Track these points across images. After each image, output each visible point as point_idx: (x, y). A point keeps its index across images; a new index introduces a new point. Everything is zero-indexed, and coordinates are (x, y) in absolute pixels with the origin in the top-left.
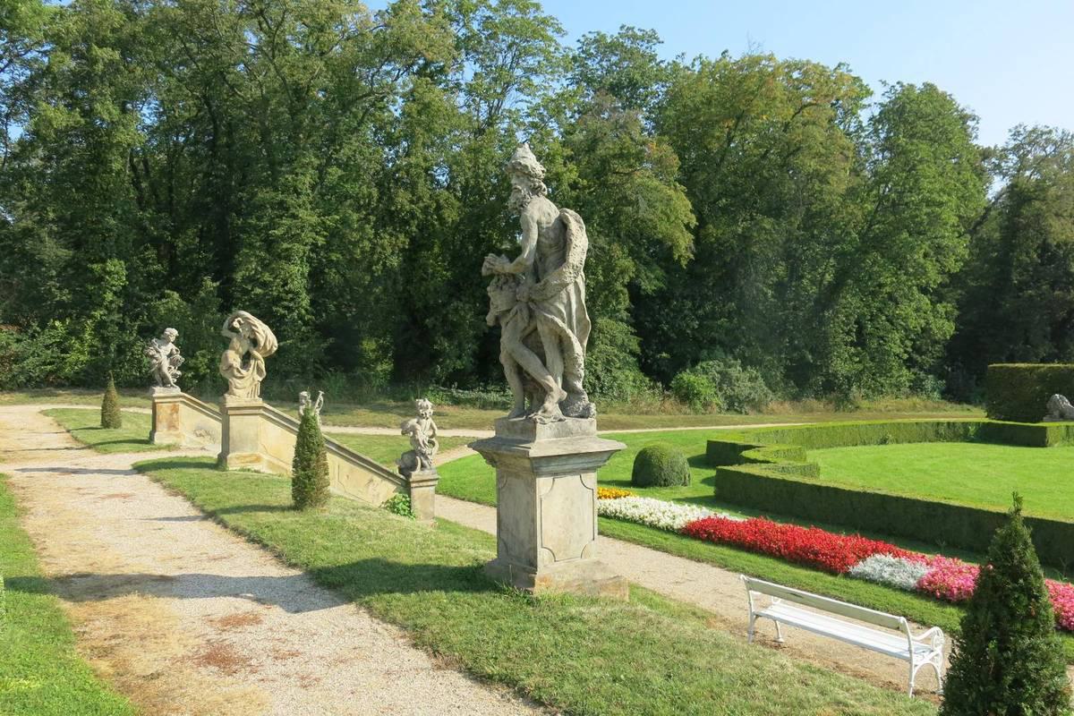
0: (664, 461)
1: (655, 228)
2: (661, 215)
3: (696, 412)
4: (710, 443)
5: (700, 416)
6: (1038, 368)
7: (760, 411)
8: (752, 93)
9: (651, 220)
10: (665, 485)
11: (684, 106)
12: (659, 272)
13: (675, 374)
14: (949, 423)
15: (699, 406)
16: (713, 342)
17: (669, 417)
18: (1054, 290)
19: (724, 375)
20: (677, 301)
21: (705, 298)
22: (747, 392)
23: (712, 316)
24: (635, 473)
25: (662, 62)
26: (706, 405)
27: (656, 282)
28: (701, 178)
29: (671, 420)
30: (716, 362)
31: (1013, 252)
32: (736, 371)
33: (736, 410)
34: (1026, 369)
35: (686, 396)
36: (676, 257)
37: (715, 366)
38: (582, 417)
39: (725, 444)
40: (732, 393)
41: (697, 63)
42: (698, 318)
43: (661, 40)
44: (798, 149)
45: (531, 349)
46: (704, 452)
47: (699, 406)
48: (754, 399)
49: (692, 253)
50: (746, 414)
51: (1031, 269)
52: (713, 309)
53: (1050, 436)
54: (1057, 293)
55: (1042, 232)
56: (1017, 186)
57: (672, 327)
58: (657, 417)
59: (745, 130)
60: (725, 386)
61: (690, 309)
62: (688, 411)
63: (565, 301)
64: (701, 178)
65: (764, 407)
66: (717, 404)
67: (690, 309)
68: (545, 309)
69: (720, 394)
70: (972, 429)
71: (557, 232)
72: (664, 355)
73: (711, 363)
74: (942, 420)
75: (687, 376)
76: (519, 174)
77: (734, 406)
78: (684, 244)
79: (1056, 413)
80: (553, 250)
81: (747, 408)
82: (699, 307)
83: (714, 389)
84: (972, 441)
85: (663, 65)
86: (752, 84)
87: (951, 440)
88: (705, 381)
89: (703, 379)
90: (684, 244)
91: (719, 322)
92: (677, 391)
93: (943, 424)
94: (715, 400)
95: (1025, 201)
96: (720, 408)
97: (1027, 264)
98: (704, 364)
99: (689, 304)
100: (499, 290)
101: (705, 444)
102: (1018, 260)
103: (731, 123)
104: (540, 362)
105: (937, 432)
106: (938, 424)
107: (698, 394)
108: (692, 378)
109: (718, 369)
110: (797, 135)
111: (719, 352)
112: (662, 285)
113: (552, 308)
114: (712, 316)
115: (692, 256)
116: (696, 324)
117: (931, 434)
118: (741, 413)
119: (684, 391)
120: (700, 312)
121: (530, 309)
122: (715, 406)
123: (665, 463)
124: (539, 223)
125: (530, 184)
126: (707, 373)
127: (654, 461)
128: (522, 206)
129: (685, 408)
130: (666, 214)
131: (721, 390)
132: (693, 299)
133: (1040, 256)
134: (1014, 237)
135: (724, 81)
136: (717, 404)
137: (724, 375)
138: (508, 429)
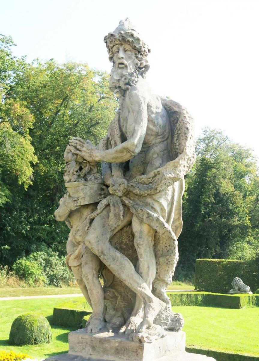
0: (34, 325)
1: (15, 161)
2: (19, 153)
3: (29, 285)
4: (55, 310)
5: (32, 288)
6: (223, 261)
7: (69, 285)
8: (73, 85)
9: (12, 156)
10: (35, 343)
11: (28, 88)
12: (7, 192)
13: (15, 261)
14: (187, 294)
15: (31, 282)
16: (39, 239)
17: (12, 289)
18: (221, 218)
19: (48, 262)
20: (17, 211)
21: (35, 211)
22: (61, 273)
23: (39, 222)
24: (12, 335)
25: (14, 57)
26: (36, 281)
27: (5, 198)
28: (38, 133)
29: (14, 292)
30: (43, 253)
31: (202, 196)
32: (54, 259)
33: (54, 285)
34: (216, 262)
35: (23, 275)
36: (20, 183)
37: (42, 255)
38: (171, 329)
39: (66, 311)
40: (52, 274)
41: (35, 63)
42: (31, 223)
43: (15, 43)
44: (98, 123)
45: (121, 249)
46: (52, 314)
47: (31, 282)
48: (65, 278)
49: (32, 181)
50: (61, 287)
51: (210, 206)
52: (39, 218)
53: (242, 302)
54: (223, 220)
55: (217, 187)
56: (205, 160)
57: (12, 230)
58: (4, 289)
59: (66, 107)
60: (48, 269)
61: (25, 218)
62: (25, 285)
63: (169, 198)
64: (38, 133)
65: (71, 283)
66: (43, 281)
67: (25, 218)
68: (147, 205)
69: (44, 274)
70: (200, 298)
71: (165, 119)
72: (7, 247)
73: (39, 253)
74: (183, 293)
75: (24, 262)
76: (128, 47)
77: (53, 282)
78: (26, 176)
79: (237, 288)
80: (158, 140)
81: (61, 283)
82: (30, 217)
83: (41, 271)
84: (200, 305)
85: (15, 60)
86: (73, 79)
87: (188, 305)
88: (36, 266)
89: (35, 264)
90: (26, 176)
91: (43, 227)
92: (17, 271)
93: (184, 295)
94: (42, 278)
95: (209, 168)
96: (44, 283)
97: (209, 203)
98: (35, 254)
99: (25, 215)
100: (82, 181)
101: (53, 310)
102: (205, 200)
103: (60, 102)
104: (133, 267)
105: (181, 300)
106: (182, 295)
107: (31, 274)
108: (28, 263)
109: (44, 257)
110: (97, 115)
111: (44, 246)
112: (8, 200)
113: (156, 206)
114: (39, 222)
115: (31, 183)
116: (28, 227)
117: (178, 301)
118: (57, 286)
119: (22, 271)
120: (31, 220)
121: (124, 205)
122: (41, 282)
123: (36, 328)
124: (149, 106)
125: (137, 61)
126: (36, 260)
127: (28, 326)
128: (128, 84)
129: (22, 283)
130: (21, 153)
131: (45, 271)
132: (27, 211)
133: (215, 199)
134: (203, 187)
135: (54, 76)
136: (43, 281)
137: (48, 262)
138: (93, 348)
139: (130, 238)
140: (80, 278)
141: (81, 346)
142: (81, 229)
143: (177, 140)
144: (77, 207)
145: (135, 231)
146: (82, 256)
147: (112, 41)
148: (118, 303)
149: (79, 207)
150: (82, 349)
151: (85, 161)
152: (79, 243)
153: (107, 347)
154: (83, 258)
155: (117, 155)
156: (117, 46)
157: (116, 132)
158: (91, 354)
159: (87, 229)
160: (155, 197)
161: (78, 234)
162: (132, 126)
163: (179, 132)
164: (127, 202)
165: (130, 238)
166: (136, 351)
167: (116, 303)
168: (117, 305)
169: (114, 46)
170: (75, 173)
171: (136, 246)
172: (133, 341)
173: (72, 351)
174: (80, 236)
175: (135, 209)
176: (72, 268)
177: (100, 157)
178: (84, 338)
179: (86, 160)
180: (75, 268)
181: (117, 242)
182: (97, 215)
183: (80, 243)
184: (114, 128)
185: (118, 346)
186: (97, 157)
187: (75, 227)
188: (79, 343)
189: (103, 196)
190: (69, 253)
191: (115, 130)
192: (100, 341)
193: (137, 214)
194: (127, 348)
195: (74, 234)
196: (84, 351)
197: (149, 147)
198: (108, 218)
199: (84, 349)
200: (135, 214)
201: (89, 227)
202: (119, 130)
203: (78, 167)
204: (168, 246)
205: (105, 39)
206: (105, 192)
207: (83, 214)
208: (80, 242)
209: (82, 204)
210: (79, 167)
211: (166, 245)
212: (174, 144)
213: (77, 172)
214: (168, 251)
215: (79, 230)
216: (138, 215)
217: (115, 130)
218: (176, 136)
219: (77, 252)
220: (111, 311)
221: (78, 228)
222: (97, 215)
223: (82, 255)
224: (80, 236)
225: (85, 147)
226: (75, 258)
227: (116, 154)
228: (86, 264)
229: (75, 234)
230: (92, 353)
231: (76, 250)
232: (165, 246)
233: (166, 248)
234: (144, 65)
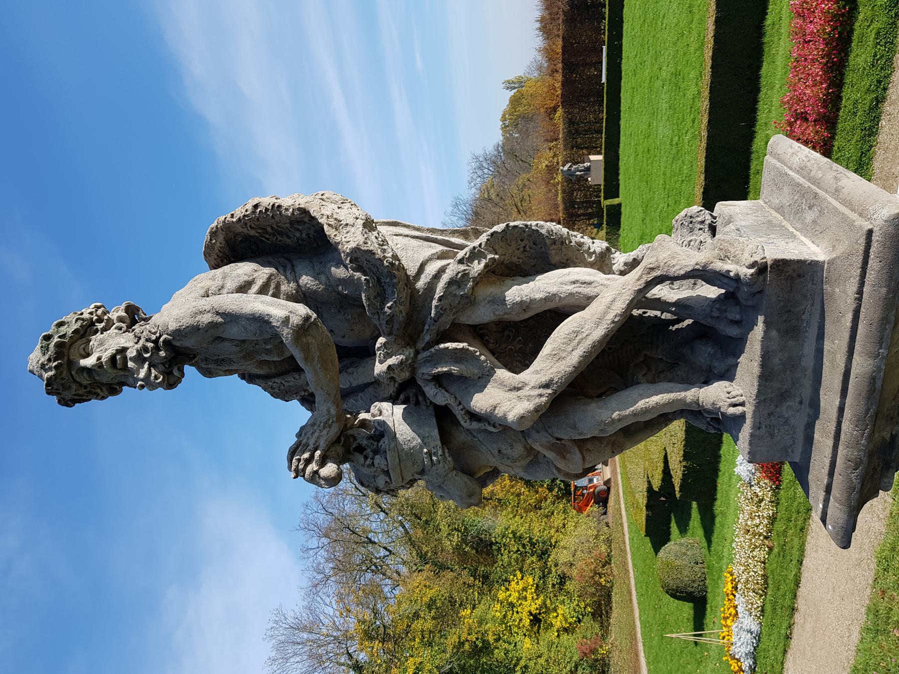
138: (783, 396)
139: (511, 334)
140: (610, 446)
141: (779, 430)
142: (494, 446)
143: (289, 237)
144: (447, 455)
145: (492, 315)
146: (558, 439)
147: (62, 384)
148: (660, 357)
149: (446, 451)
150: (786, 427)
151: (342, 439)
152: (530, 450)
153: (780, 360)
154: (562, 437)
155: (316, 359)
156: (73, 373)
157: (291, 384)
158: (801, 403)
159: (494, 427)
160: (412, 271)
161: (509, 451)
162: (248, 327)
163: (269, 229)
164: (427, 338)
165: (511, 334)
166: (791, 278)
167: (661, 359)
168: (664, 358)
169: (75, 381)
170: (369, 461)
171: (527, 316)
172: (760, 292)
173: (793, 452)
174: (512, 446)
175: (442, 314)
176: (588, 466)
177: (330, 404)
178: (760, 423)
179: (339, 438)
180: (587, 458)
181: (520, 362)
182: (460, 404)
183: (528, 447)
184: (282, 388)
185: (778, 330)
186: (328, 411)
187: (494, 460)
188: (772, 436)
189: (420, 399)
190: (554, 474)
191: (286, 384)
192: (766, 380)
193: (451, 309)
194: (782, 304)
195: (509, 462)
196: (792, 421)
197: (304, 295)
198: (466, 378)
199: (786, 422)
200: (454, 314)
201: (489, 424)
202: (284, 377)
203: (357, 455)
204: (523, 244)
205: (68, 406)
206: (411, 395)
207: (464, 444)
208: (525, 447)
209: (439, 443)
210: (356, 454)
211: (522, 249)
212: (300, 245)
213: (366, 458)
214: (534, 244)
215: (499, 451)
216: (455, 307)
217: (286, 384)
218: (279, 238)
219: (550, 455)
220: (678, 373)
221: (496, 453)
222: (460, 404)
223: (555, 441)
224: (512, 446)
225: (308, 439)
226: (564, 457)
227: (313, 359)
228: (574, 427)
229: (508, 458)
230: (797, 400)
231: (545, 456)
232: (525, 251)
233: (528, 248)
234: (124, 314)
